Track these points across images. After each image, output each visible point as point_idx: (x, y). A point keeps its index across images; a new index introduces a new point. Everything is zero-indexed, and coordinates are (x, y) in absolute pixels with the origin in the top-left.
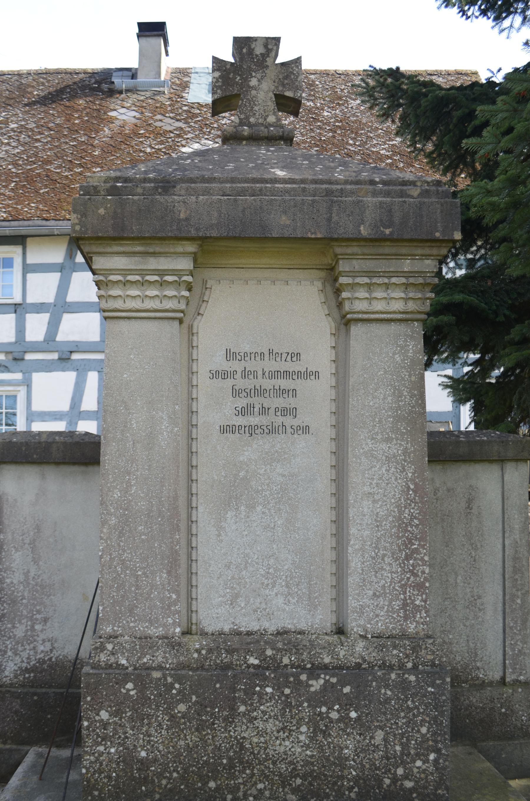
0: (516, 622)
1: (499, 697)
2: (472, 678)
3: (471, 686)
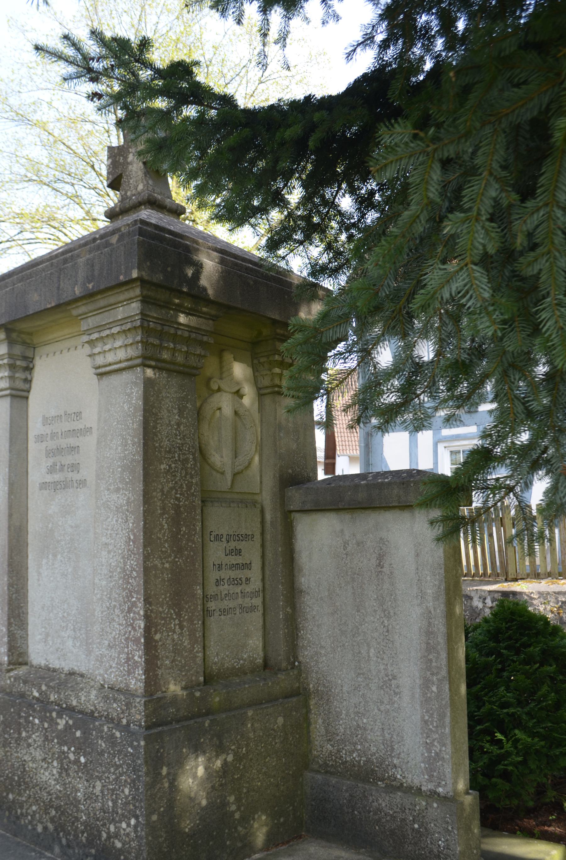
0: (431, 716)
1: (411, 807)
2: (389, 777)
3: (387, 786)
